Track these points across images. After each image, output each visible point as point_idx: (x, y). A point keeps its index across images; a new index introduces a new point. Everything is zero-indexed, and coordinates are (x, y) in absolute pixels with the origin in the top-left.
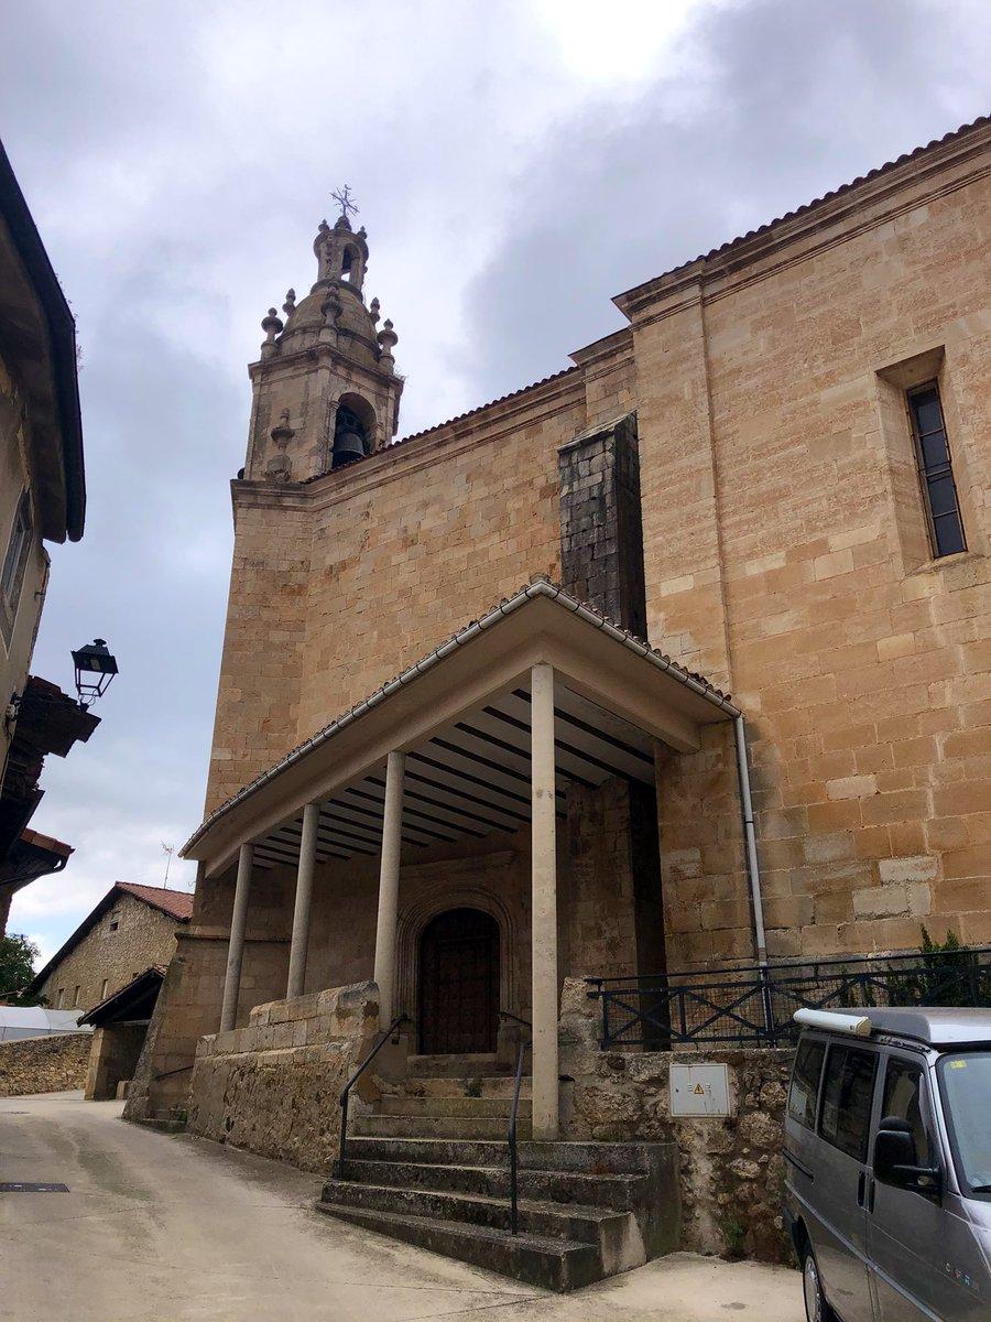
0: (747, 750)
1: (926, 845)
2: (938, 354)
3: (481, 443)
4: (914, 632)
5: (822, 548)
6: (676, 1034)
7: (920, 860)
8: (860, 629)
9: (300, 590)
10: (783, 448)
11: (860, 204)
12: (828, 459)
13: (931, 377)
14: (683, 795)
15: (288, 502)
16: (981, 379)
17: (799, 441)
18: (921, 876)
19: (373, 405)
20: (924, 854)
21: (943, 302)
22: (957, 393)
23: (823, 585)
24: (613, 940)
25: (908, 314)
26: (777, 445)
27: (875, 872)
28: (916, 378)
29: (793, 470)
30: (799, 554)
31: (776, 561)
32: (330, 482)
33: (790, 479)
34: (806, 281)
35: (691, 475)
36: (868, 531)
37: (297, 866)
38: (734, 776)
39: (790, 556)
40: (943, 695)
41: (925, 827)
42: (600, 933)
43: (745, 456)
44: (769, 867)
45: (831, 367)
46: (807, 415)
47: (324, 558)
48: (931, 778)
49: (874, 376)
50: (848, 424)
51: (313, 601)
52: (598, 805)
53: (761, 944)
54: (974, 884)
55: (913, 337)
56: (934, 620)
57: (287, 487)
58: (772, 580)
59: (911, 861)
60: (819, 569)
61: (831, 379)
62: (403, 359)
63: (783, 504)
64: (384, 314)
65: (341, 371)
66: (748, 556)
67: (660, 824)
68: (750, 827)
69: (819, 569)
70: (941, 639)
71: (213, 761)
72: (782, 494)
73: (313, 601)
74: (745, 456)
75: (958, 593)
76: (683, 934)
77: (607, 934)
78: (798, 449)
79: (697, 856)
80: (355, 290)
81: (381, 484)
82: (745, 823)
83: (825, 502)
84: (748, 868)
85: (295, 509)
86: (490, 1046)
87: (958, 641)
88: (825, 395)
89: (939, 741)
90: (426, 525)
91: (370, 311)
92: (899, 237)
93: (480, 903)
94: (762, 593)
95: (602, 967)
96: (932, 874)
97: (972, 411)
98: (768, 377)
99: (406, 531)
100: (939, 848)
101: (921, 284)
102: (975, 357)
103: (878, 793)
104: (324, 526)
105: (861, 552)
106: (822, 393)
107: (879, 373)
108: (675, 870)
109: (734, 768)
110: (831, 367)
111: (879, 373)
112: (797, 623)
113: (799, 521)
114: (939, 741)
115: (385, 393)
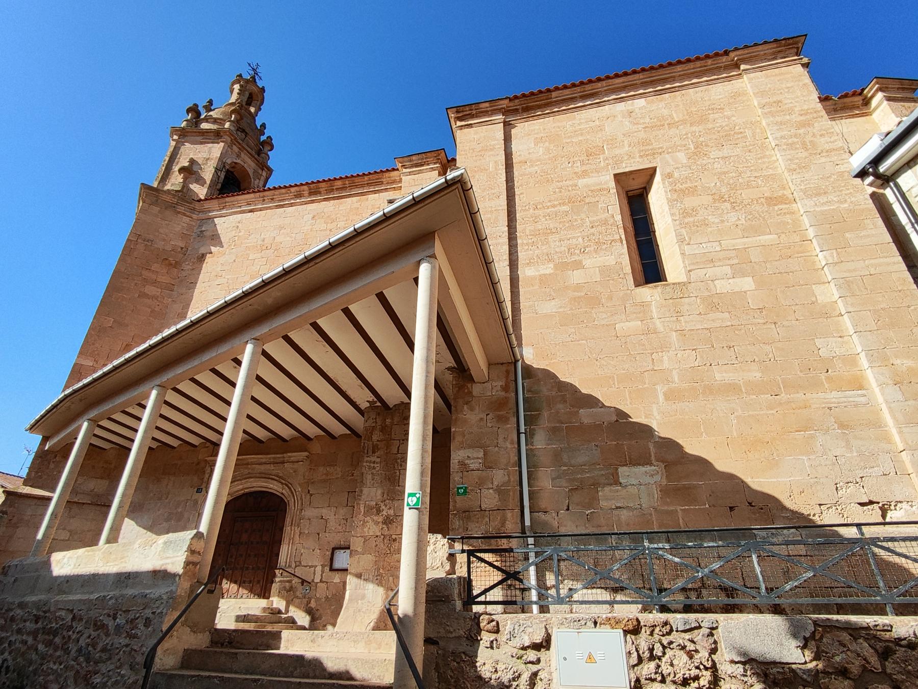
0: (523, 384)
1: (653, 458)
2: (652, 172)
3: (325, 200)
4: (641, 321)
5: (578, 265)
6: (553, 597)
7: (648, 468)
8: (604, 316)
9: (177, 265)
10: (554, 206)
11: (605, 90)
12: (583, 216)
13: (643, 186)
14: (472, 409)
15: (181, 209)
16: (680, 186)
17: (564, 204)
18: (648, 480)
19: (252, 176)
20: (651, 464)
21: (656, 145)
22: (657, 200)
23: (578, 287)
24: (388, 517)
25: (634, 148)
26: (549, 204)
27: (615, 476)
28: (636, 184)
29: (560, 219)
30: (563, 267)
31: (548, 269)
32: (214, 204)
33: (558, 224)
34: (570, 123)
35: (491, 212)
36: (610, 260)
37: (130, 450)
38: (513, 401)
39: (556, 267)
40: (662, 361)
41: (651, 446)
42: (379, 511)
43: (527, 207)
44: (535, 466)
45: (584, 168)
46: (569, 191)
47: (199, 248)
48: (655, 413)
49: (612, 177)
50: (597, 199)
51: (184, 274)
52: (388, 421)
53: (528, 523)
54: (687, 488)
55: (638, 159)
56: (655, 315)
57: (183, 200)
58: (543, 280)
59: (642, 469)
60: (576, 277)
61: (585, 174)
62: (274, 159)
63: (551, 238)
64: (268, 133)
65: (235, 148)
66: (528, 264)
67: (453, 430)
68: (523, 437)
69: (576, 277)
70: (659, 325)
71: (75, 365)
72: (549, 232)
73: (184, 274)
74: (527, 207)
75: (671, 301)
76: (464, 512)
77: (384, 513)
78: (565, 208)
79: (481, 455)
80: (253, 117)
81: (251, 211)
82: (519, 433)
83: (580, 239)
84: (520, 466)
85: (185, 215)
86: (264, 593)
87: (671, 330)
88: (581, 182)
89: (660, 390)
90: (278, 239)
91: (259, 128)
92: (628, 110)
93: (274, 487)
94: (536, 287)
95: (377, 536)
96: (657, 478)
97: (675, 202)
98: (545, 168)
99: (264, 241)
100: (663, 462)
101: (642, 135)
102: (676, 175)
103: (617, 421)
104: (203, 229)
105: (605, 270)
106: (579, 181)
107: (616, 175)
108: (462, 464)
109: (513, 394)
110: (584, 168)
111: (616, 175)
112: (561, 307)
113: (563, 248)
114: (660, 390)
115: (260, 172)
